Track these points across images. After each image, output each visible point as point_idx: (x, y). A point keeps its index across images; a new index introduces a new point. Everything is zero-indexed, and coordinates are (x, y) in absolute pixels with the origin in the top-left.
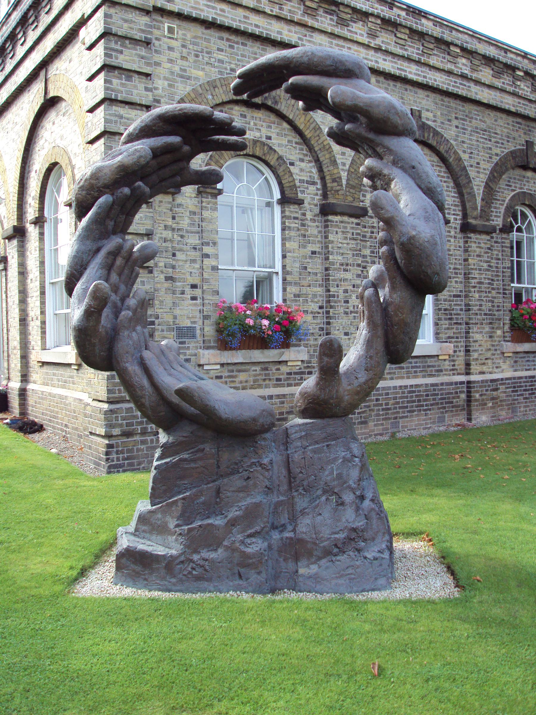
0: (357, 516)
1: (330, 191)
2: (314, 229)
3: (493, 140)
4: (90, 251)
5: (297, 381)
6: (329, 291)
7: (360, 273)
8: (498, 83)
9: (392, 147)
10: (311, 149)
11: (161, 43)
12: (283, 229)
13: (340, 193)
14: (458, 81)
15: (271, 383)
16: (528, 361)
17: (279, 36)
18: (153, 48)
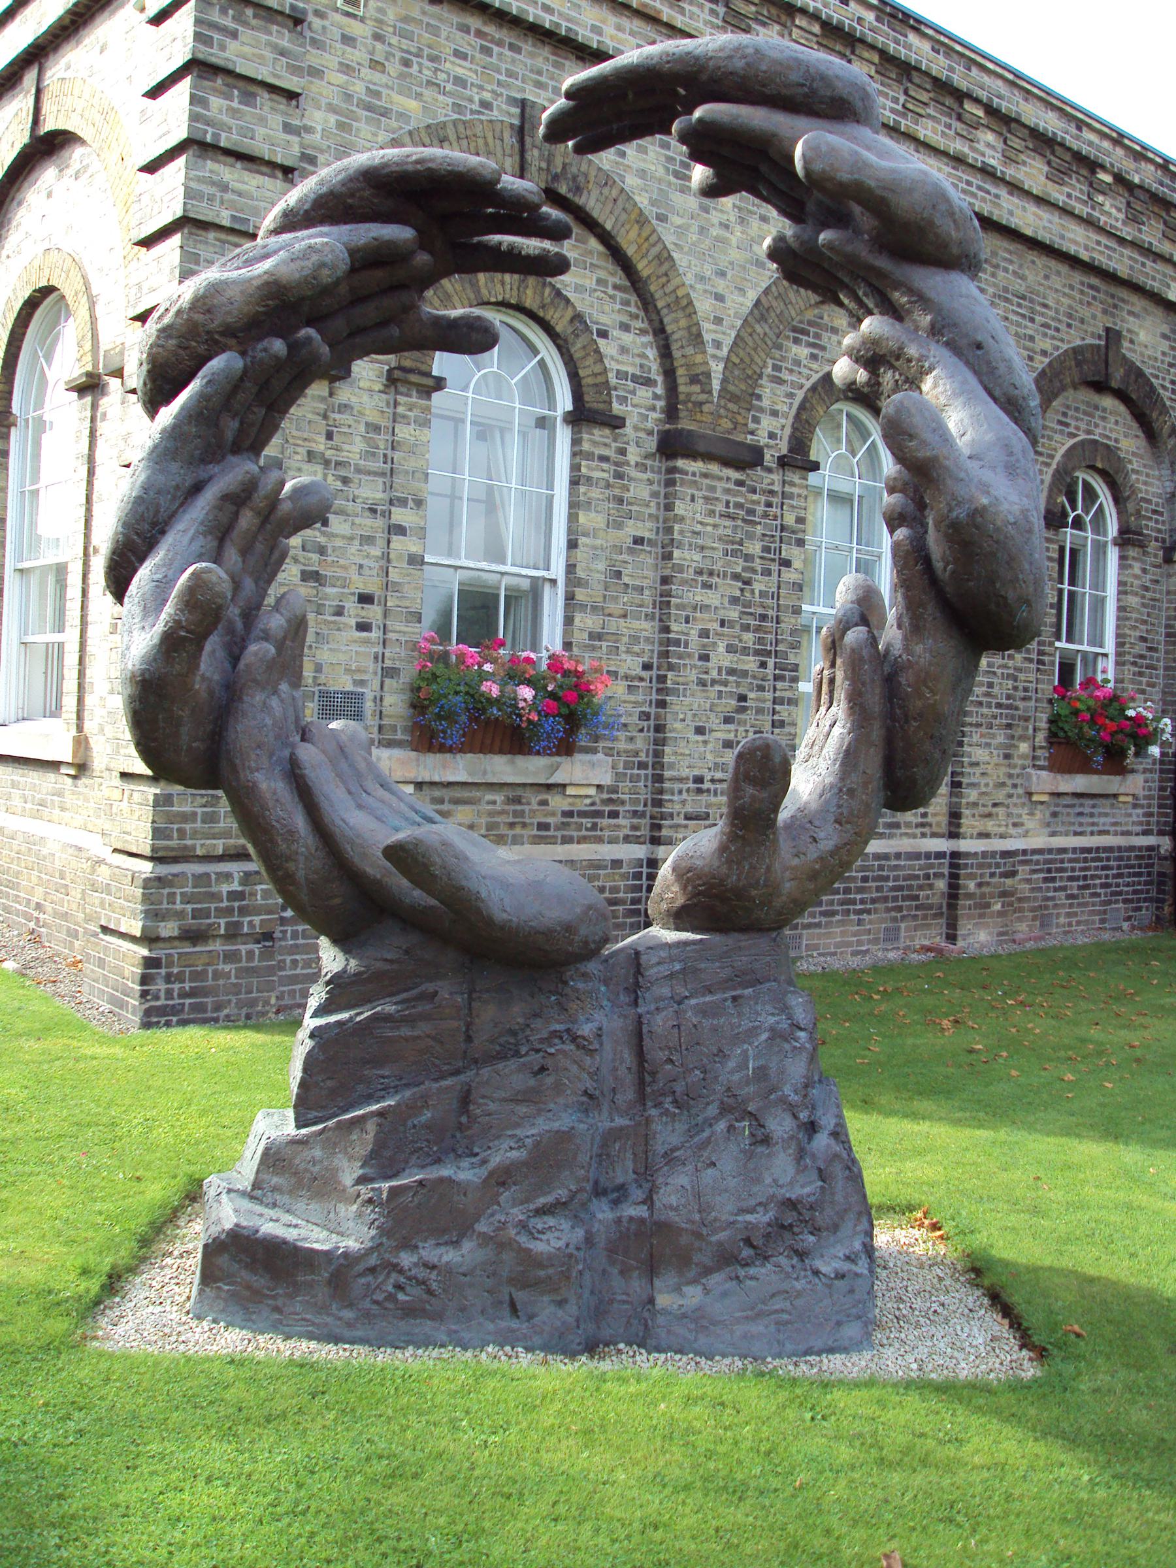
0: (798, 1172)
1: (685, 403)
2: (642, 487)
3: (1038, 318)
4: (177, 487)
5: (584, 833)
6: (666, 629)
7: (738, 593)
8: (1058, 194)
9: (931, 294)
10: (647, 303)
11: (326, 23)
12: (574, 482)
13: (706, 408)
14: (975, 181)
15: (526, 832)
16: (1080, 814)
17: (596, 38)
18: (308, 34)
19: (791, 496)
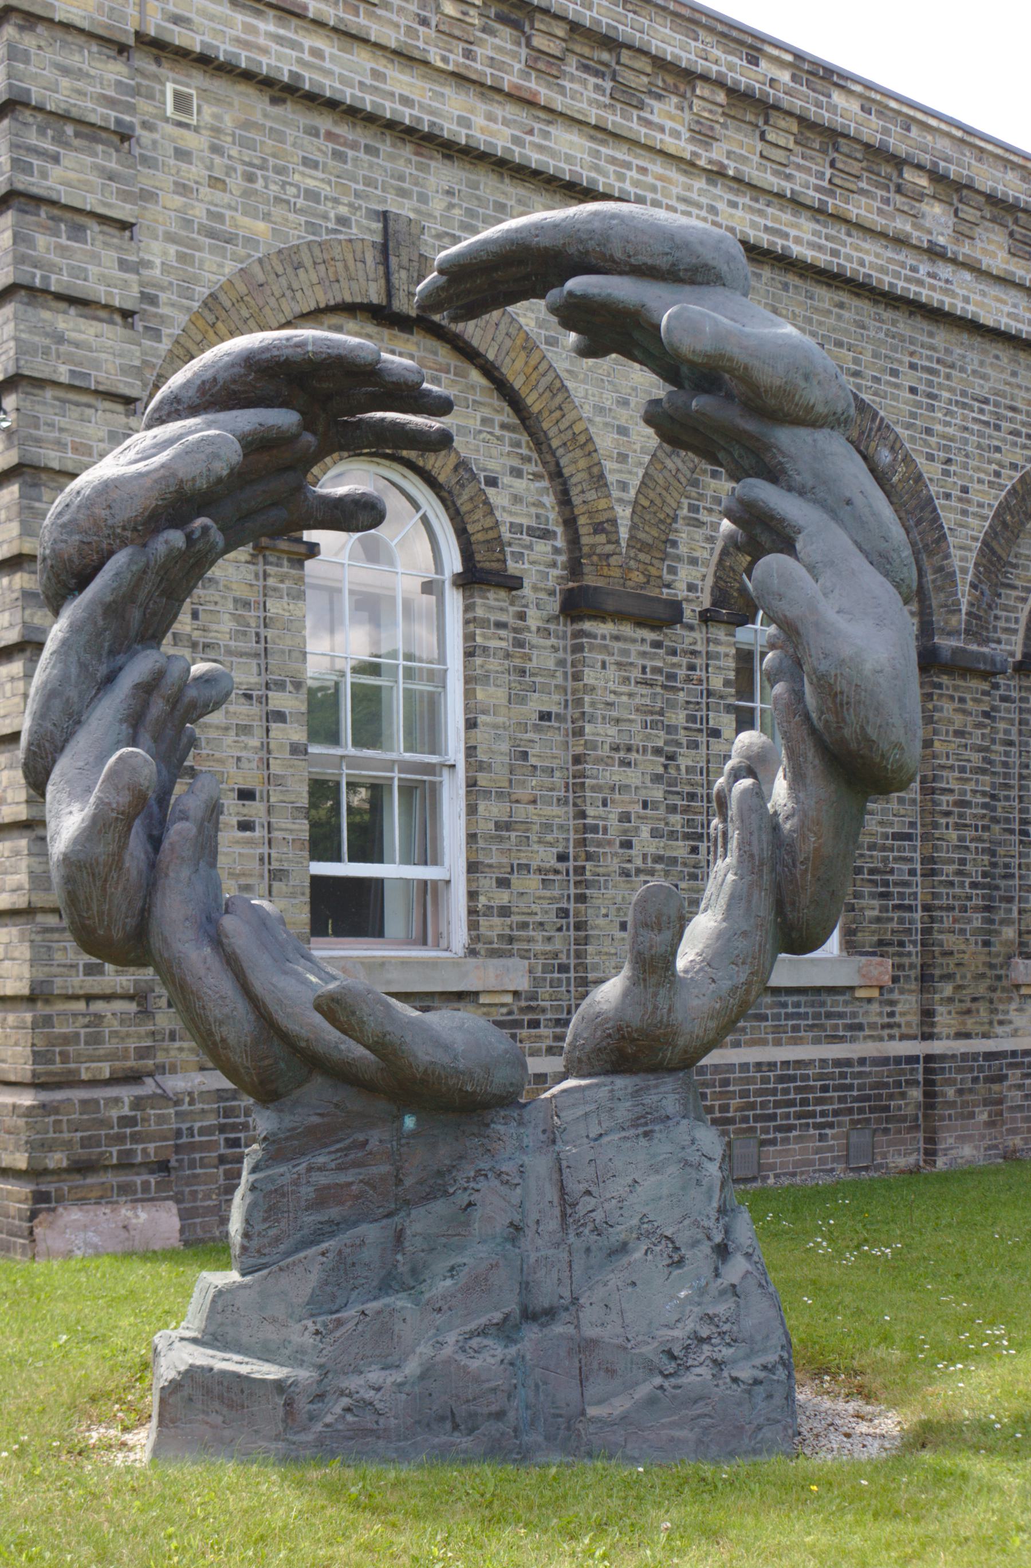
2: (544, 657)
3: (1004, 424)
6: (583, 815)
7: (661, 770)
10: (539, 442)
11: (156, 136)
12: (469, 654)
13: (613, 561)
18: (137, 151)
19: (717, 656)
